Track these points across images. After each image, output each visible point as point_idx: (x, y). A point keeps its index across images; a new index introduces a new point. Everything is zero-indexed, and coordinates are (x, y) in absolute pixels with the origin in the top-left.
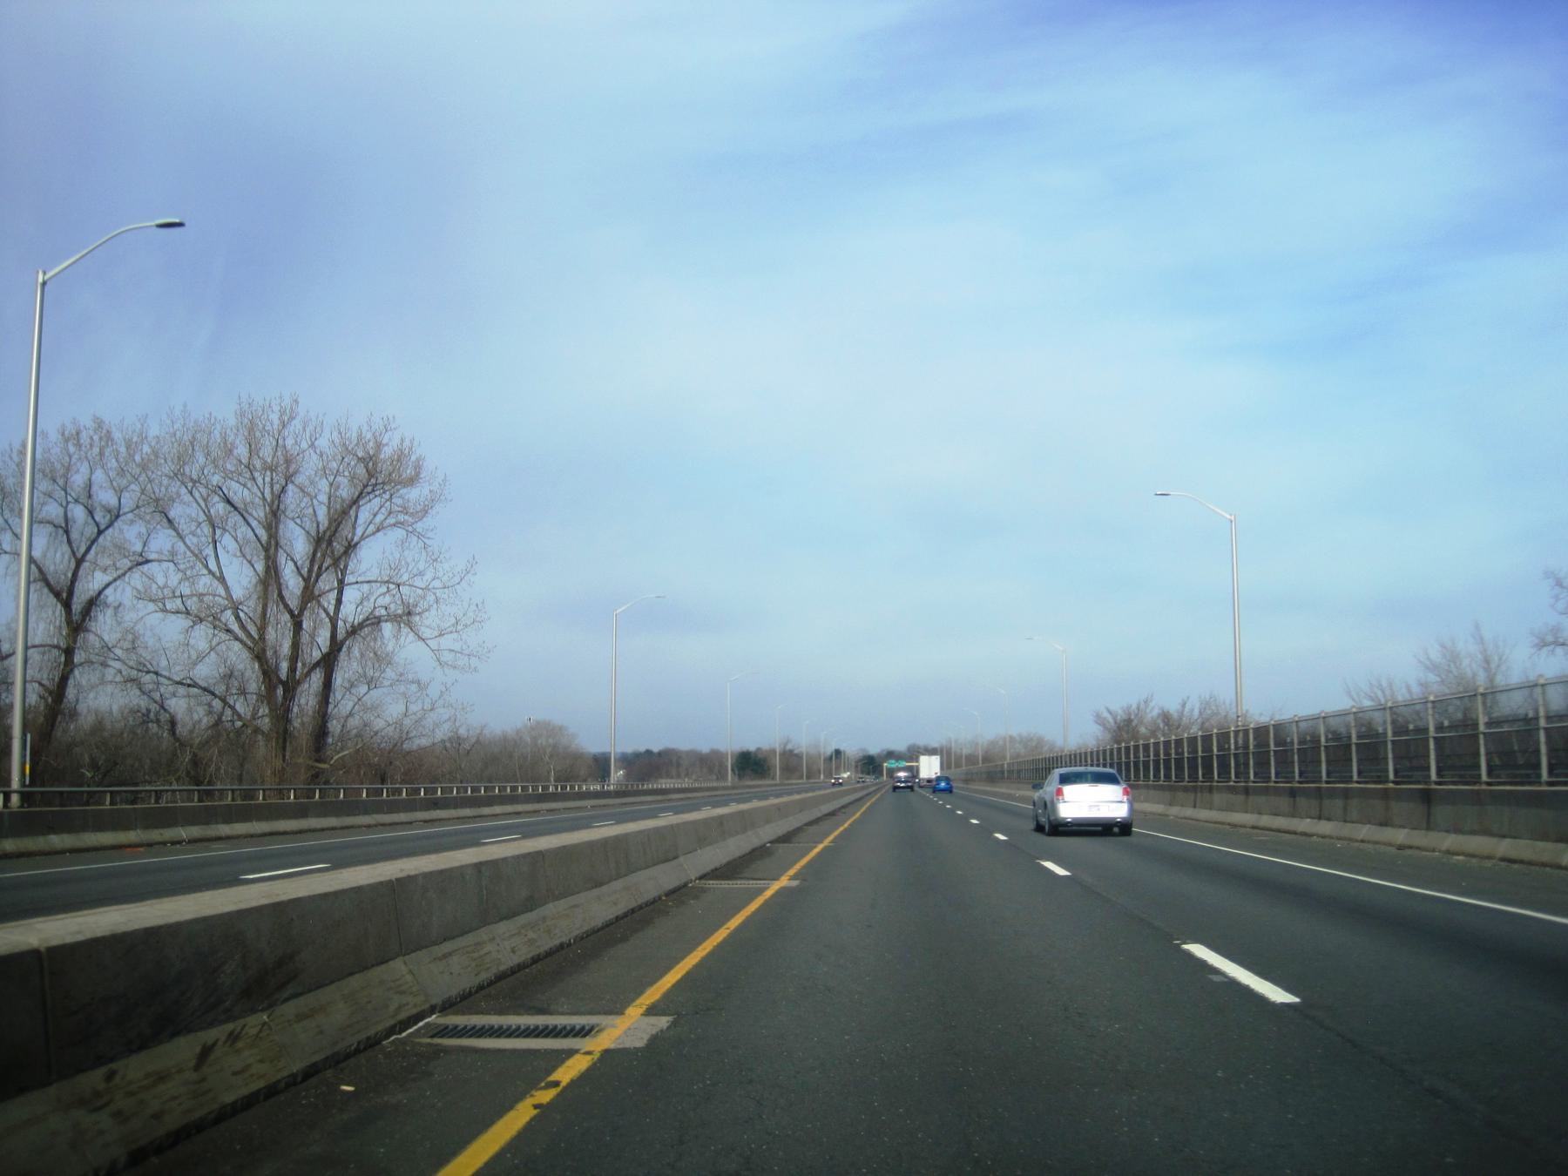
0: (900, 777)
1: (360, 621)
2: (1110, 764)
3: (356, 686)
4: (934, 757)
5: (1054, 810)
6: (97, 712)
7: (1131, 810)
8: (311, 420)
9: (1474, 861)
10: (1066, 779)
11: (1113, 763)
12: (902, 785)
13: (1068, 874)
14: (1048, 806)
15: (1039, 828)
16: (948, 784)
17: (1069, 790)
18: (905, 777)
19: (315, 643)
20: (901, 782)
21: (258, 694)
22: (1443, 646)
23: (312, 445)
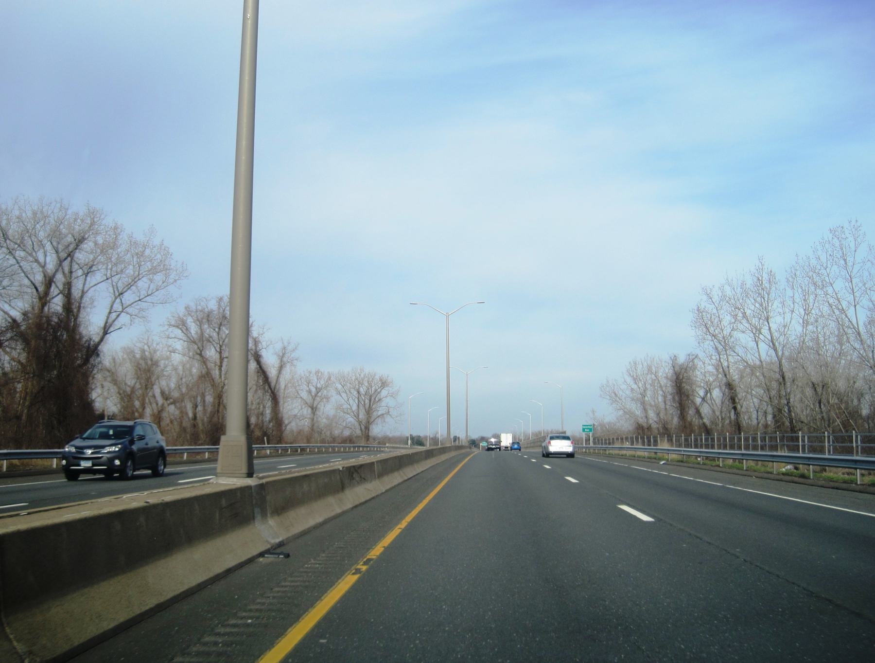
0: (492, 442)
1: (209, 409)
2: (705, 445)
3: (79, 246)
4: (509, 434)
5: (548, 448)
6: (113, 412)
7: (574, 448)
8: (697, 356)
9: (28, 398)
10: (552, 438)
11: (708, 445)
12: (494, 447)
13: (577, 481)
14: (546, 448)
15: (544, 456)
16: (519, 446)
17: (553, 442)
18: (495, 442)
19: (723, 344)
20: (492, 445)
21: (150, 414)
22: (103, 411)
23: (262, 402)
